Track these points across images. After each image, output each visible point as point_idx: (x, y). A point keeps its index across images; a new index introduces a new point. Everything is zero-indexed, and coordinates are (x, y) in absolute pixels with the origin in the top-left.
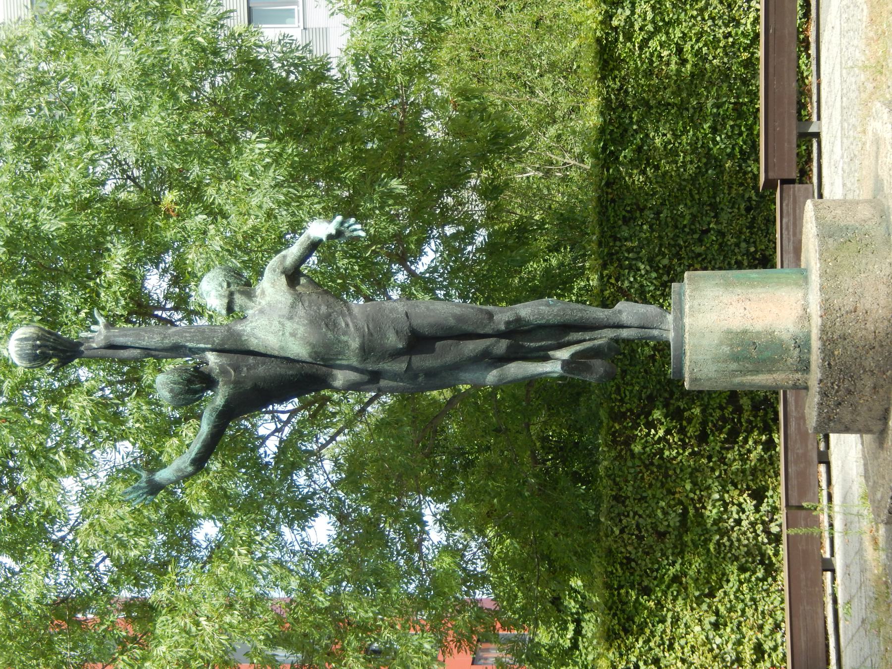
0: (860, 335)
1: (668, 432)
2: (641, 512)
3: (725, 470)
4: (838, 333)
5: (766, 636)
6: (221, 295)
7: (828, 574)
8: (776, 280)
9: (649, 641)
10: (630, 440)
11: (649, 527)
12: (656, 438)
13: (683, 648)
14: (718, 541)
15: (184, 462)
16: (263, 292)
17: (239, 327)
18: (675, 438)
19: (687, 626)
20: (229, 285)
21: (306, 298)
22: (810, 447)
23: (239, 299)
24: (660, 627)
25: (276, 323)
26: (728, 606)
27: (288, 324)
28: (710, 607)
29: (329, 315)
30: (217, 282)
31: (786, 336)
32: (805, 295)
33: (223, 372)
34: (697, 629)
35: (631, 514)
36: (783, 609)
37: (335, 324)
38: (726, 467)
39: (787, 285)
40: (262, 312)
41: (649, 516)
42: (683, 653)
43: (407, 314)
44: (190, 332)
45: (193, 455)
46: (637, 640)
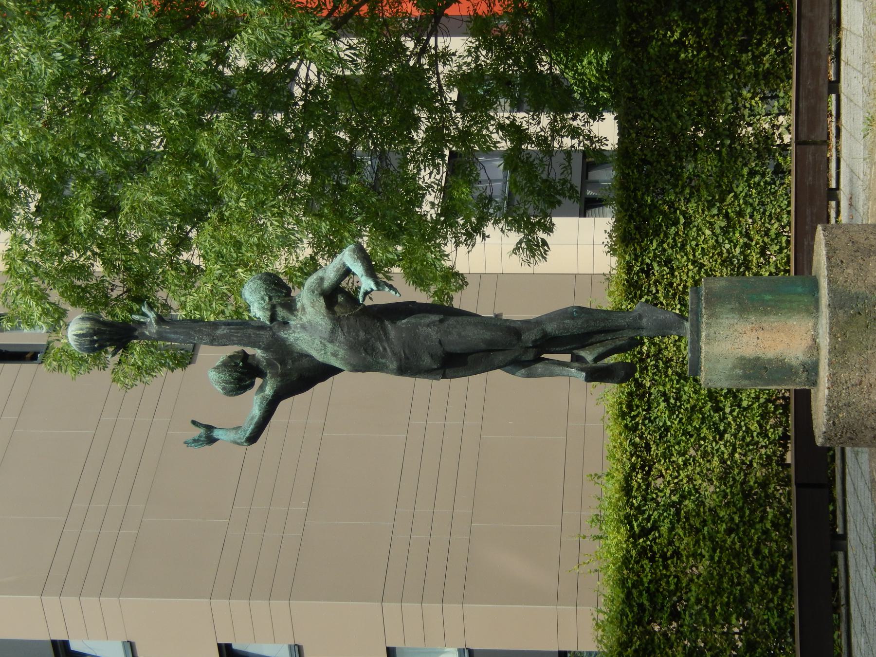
0: (863, 403)
1: (684, 34)
2: (656, 115)
3: (739, 74)
4: (844, 402)
5: (772, 240)
6: (263, 308)
7: (833, 204)
8: (788, 305)
9: (663, 242)
10: (645, 43)
11: (664, 130)
12: (672, 40)
13: (694, 250)
14: (730, 146)
15: (240, 438)
16: (303, 309)
17: (283, 334)
18: (691, 40)
19: (699, 229)
20: (270, 298)
21: (344, 322)
22: (821, 82)
23: (281, 312)
24: (673, 230)
25: (317, 341)
26: (738, 209)
27: (329, 346)
28: (720, 210)
29: (367, 341)
30: (259, 296)
31: (794, 362)
32: (816, 324)
33: (270, 364)
34: (708, 232)
35: (647, 117)
36: (789, 213)
37: (374, 349)
38: (739, 71)
39: (799, 312)
40: (303, 327)
41: (665, 120)
42: (694, 255)
43: (440, 342)
44: (237, 337)
45: (248, 435)
46: (652, 243)
